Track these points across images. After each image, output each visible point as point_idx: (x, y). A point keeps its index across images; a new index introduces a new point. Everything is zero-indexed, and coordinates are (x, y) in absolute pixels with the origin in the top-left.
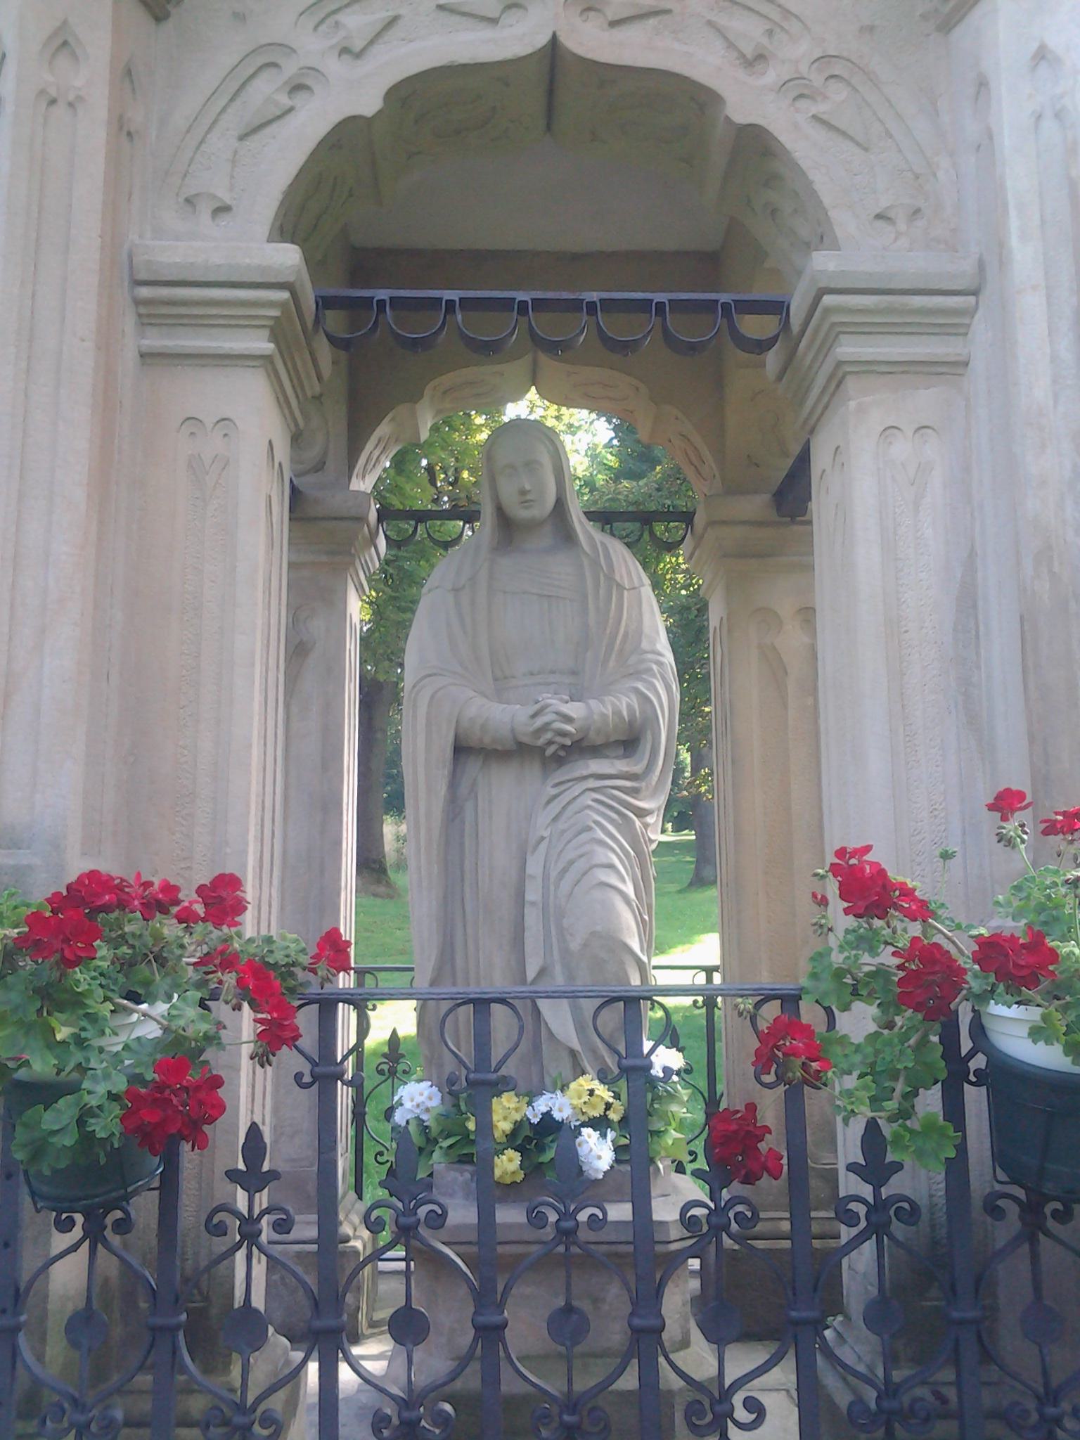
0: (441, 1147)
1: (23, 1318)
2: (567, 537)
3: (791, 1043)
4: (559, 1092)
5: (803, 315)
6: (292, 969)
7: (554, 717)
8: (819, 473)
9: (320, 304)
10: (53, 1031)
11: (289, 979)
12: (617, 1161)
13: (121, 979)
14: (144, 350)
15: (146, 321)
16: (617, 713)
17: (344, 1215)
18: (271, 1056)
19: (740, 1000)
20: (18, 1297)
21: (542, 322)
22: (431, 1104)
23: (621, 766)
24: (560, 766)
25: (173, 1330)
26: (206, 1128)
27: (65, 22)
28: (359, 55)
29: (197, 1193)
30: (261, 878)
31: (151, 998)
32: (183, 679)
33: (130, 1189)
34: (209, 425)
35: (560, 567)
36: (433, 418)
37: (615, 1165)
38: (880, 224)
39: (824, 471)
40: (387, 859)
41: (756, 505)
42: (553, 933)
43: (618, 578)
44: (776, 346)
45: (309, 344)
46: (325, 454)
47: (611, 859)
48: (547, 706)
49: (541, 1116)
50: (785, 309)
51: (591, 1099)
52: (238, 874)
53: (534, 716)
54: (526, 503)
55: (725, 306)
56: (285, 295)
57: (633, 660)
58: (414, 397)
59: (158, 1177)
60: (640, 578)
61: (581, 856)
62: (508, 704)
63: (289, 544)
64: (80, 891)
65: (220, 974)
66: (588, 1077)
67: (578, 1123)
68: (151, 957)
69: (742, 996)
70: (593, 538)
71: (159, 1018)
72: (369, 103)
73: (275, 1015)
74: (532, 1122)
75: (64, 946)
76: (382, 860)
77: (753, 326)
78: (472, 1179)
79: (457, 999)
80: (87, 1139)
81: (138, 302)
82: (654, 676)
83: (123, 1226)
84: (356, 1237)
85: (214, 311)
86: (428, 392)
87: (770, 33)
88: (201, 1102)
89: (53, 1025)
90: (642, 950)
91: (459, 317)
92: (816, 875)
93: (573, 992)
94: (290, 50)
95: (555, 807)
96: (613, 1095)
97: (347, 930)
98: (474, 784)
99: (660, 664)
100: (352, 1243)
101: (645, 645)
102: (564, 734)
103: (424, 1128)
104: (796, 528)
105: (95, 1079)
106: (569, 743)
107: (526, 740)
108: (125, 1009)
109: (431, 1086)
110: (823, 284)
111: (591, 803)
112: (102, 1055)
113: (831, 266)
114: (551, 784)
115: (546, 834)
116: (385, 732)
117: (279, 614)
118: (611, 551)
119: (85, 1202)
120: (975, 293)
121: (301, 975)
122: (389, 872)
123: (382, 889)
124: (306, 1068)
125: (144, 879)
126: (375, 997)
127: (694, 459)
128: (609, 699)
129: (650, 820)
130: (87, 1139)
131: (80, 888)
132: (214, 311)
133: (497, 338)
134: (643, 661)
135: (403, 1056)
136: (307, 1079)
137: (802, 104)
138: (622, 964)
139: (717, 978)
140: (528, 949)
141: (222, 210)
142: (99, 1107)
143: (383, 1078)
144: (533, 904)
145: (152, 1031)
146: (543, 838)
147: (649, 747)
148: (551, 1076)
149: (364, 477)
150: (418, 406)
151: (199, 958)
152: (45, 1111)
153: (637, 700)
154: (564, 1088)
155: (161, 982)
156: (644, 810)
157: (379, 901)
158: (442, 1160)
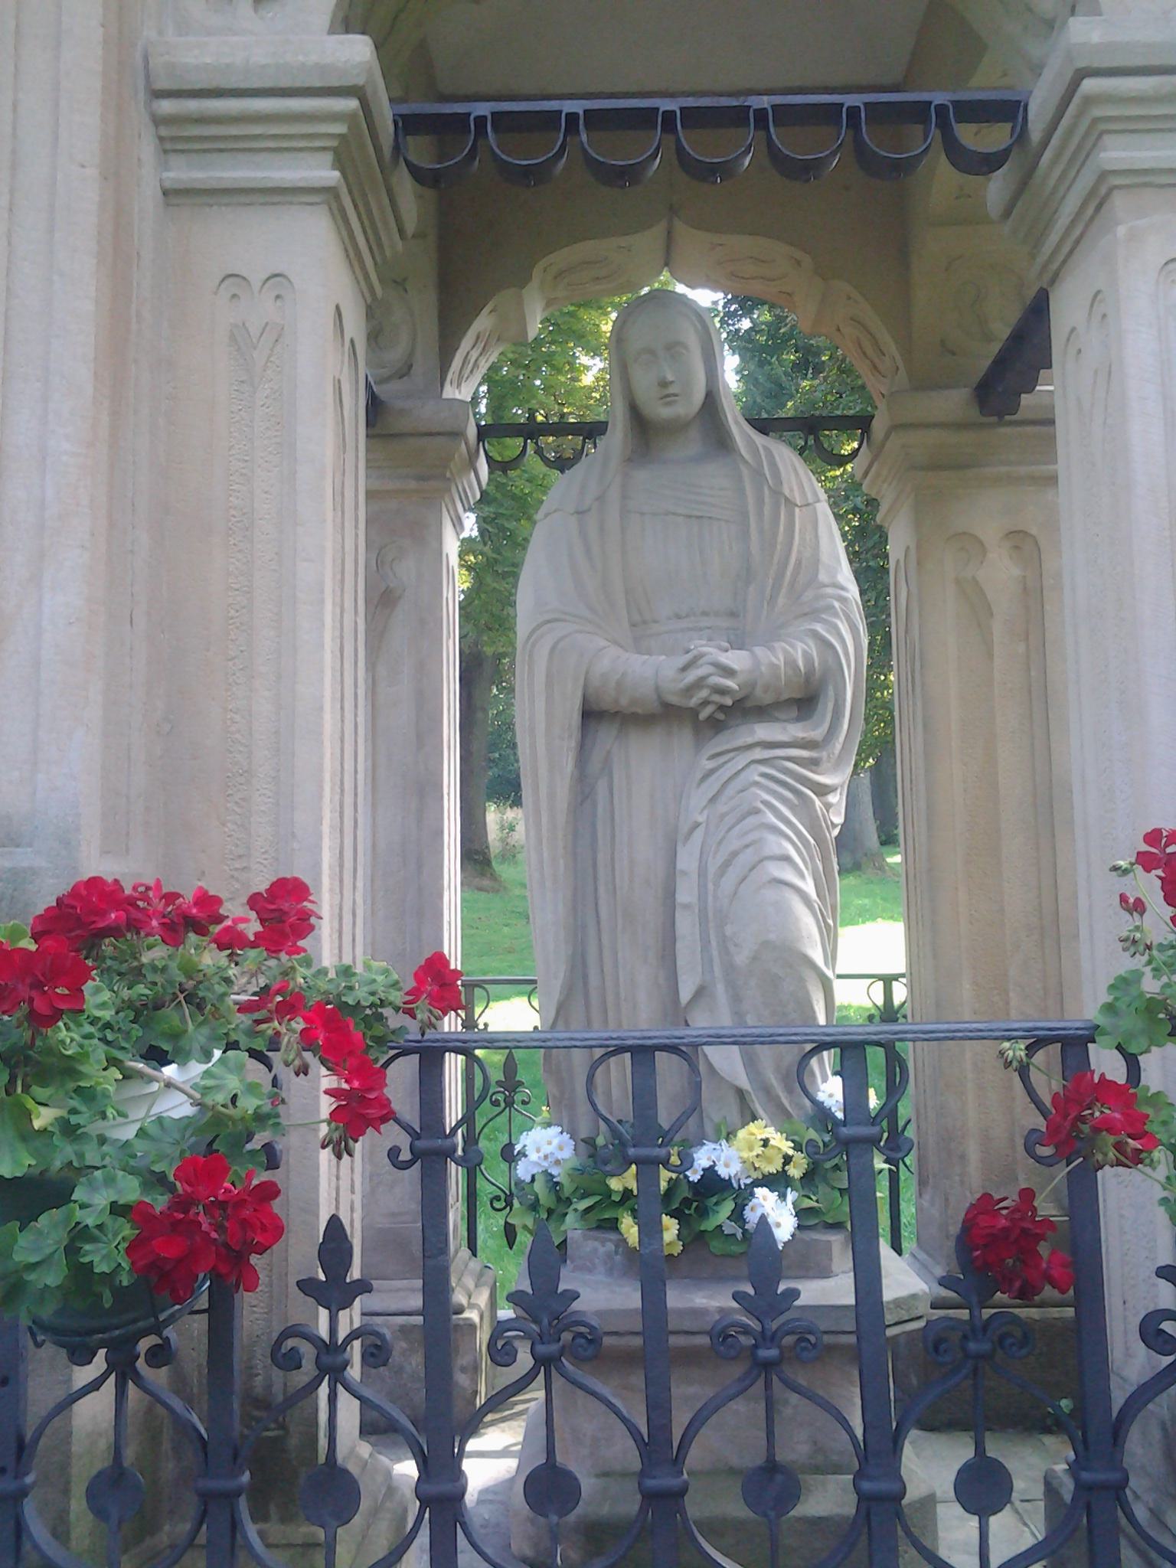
0: (576, 1210)
1: (29, 1479)
2: (719, 441)
3: (1102, 1112)
4: (724, 1142)
5: (1048, 116)
6: (380, 1010)
7: (710, 669)
8: (1067, 330)
9: (400, 124)
10: (28, 1115)
11: (376, 1025)
12: (799, 1227)
13: (137, 1031)
14: (168, 185)
15: (168, 146)
16: (791, 663)
17: (456, 1280)
18: (351, 1142)
19: (1006, 1045)
20: (22, 1449)
21: (695, 144)
22: (560, 1156)
23: (796, 731)
24: (717, 733)
25: (232, 1496)
26: (254, 1259)
29: (266, 1290)
30: (341, 881)
31: (180, 1056)
32: (231, 621)
33: (162, 1317)
34: (256, 284)
35: (713, 477)
36: (544, 310)
37: (797, 1232)
39: (1073, 330)
40: (491, 850)
41: (954, 402)
42: (714, 943)
43: (787, 492)
44: (1004, 167)
45: (386, 181)
46: (411, 354)
47: (786, 849)
48: (702, 655)
49: (702, 1173)
50: (1021, 108)
51: (766, 1150)
52: (306, 879)
53: (685, 669)
54: (667, 399)
55: (941, 109)
56: (352, 104)
57: (809, 595)
58: (523, 281)
59: (207, 1292)
60: (815, 494)
61: (747, 846)
62: (650, 654)
63: (367, 468)
64: (75, 908)
65: (276, 1023)
66: (759, 1123)
67: (748, 1181)
68: (181, 997)
69: (1009, 1039)
70: (754, 442)
71: (187, 1088)
73: (356, 1084)
74: (691, 1179)
75: (34, 994)
76: (486, 851)
77: (974, 137)
78: (616, 1253)
79: (608, 1046)
80: (81, 1274)
81: (158, 121)
82: (836, 615)
83: (160, 1355)
84: (472, 1306)
85: (257, 130)
86: (537, 273)
88: (245, 1223)
89: (28, 1107)
90: (826, 964)
91: (584, 137)
92: (1115, 869)
93: (771, 1036)
96: (792, 1145)
97: (453, 951)
98: (607, 761)
99: (843, 600)
100: (466, 1315)
101: (823, 577)
102: (722, 691)
103: (554, 1186)
104: (1002, 430)
105: (93, 1187)
106: (729, 702)
107: (674, 700)
108: (141, 1075)
109: (562, 1133)
110: (1081, 63)
111: (758, 779)
112: (105, 1148)
113: (1096, 37)
114: (706, 757)
115: (701, 819)
116: (485, 710)
117: (355, 537)
118: (777, 459)
119: (101, 1335)
121: (395, 1020)
122: (494, 864)
123: (486, 883)
124: (403, 1141)
125: (165, 890)
126: (496, 1044)
127: (870, 351)
129: (833, 798)
130: (81, 1274)
131: (74, 903)
132: (257, 130)
133: (641, 159)
134: (824, 596)
135: (521, 1083)
136: (405, 1156)
138: (801, 981)
139: (900, 992)
140: (681, 962)
142: (100, 1227)
143: (498, 1110)
144: (687, 907)
145: (178, 1107)
146: (697, 825)
147: (830, 706)
148: (712, 1120)
149: (459, 385)
150: (524, 291)
151: (254, 994)
152: (20, 1231)
153: (816, 645)
154: (730, 1136)
155: (196, 1034)
156: (825, 786)
157: (483, 895)
158: (577, 1226)
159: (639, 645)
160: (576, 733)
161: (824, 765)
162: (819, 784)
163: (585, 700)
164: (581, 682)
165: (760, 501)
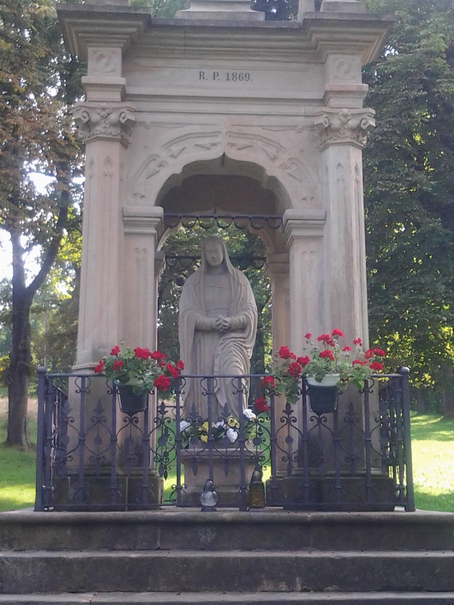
16: (240, 321)
23: (241, 335)
27: (109, 157)
28: (176, 157)
38: (304, 201)
60: (247, 282)
72: (178, 170)
87: (278, 152)
94: (158, 156)
95: (222, 346)
99: (252, 307)
101: (248, 301)
102: (225, 326)
106: (226, 328)
107: (214, 327)
110: (289, 218)
120: (325, 220)
128: (237, 317)
129: (249, 350)
137: (285, 170)
141: (143, 197)
146: (219, 355)
147: (248, 330)
159: (207, 315)
160: (193, 333)
161: (247, 343)
162: (246, 347)
163: (195, 327)
164: (195, 324)
165: (234, 284)
